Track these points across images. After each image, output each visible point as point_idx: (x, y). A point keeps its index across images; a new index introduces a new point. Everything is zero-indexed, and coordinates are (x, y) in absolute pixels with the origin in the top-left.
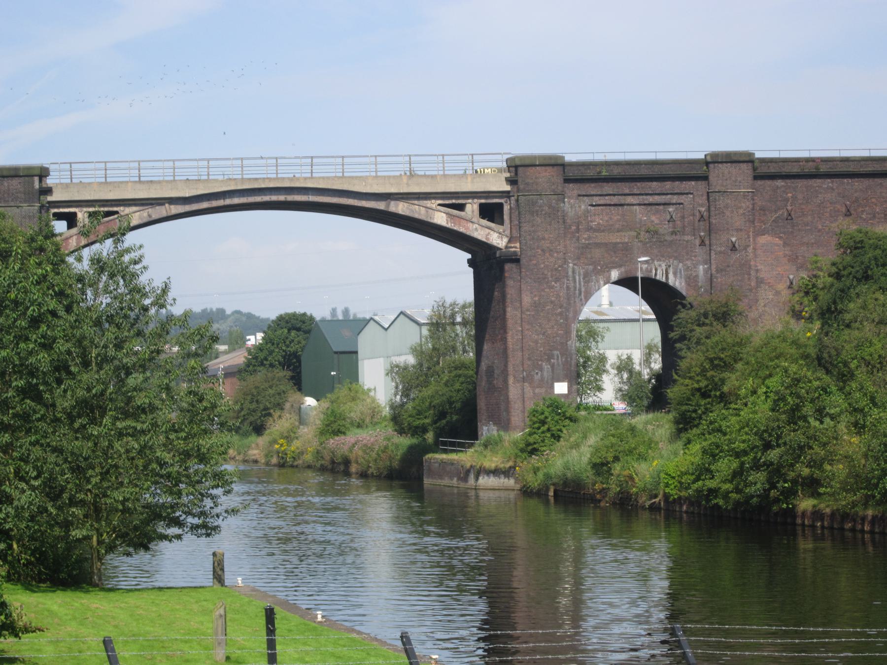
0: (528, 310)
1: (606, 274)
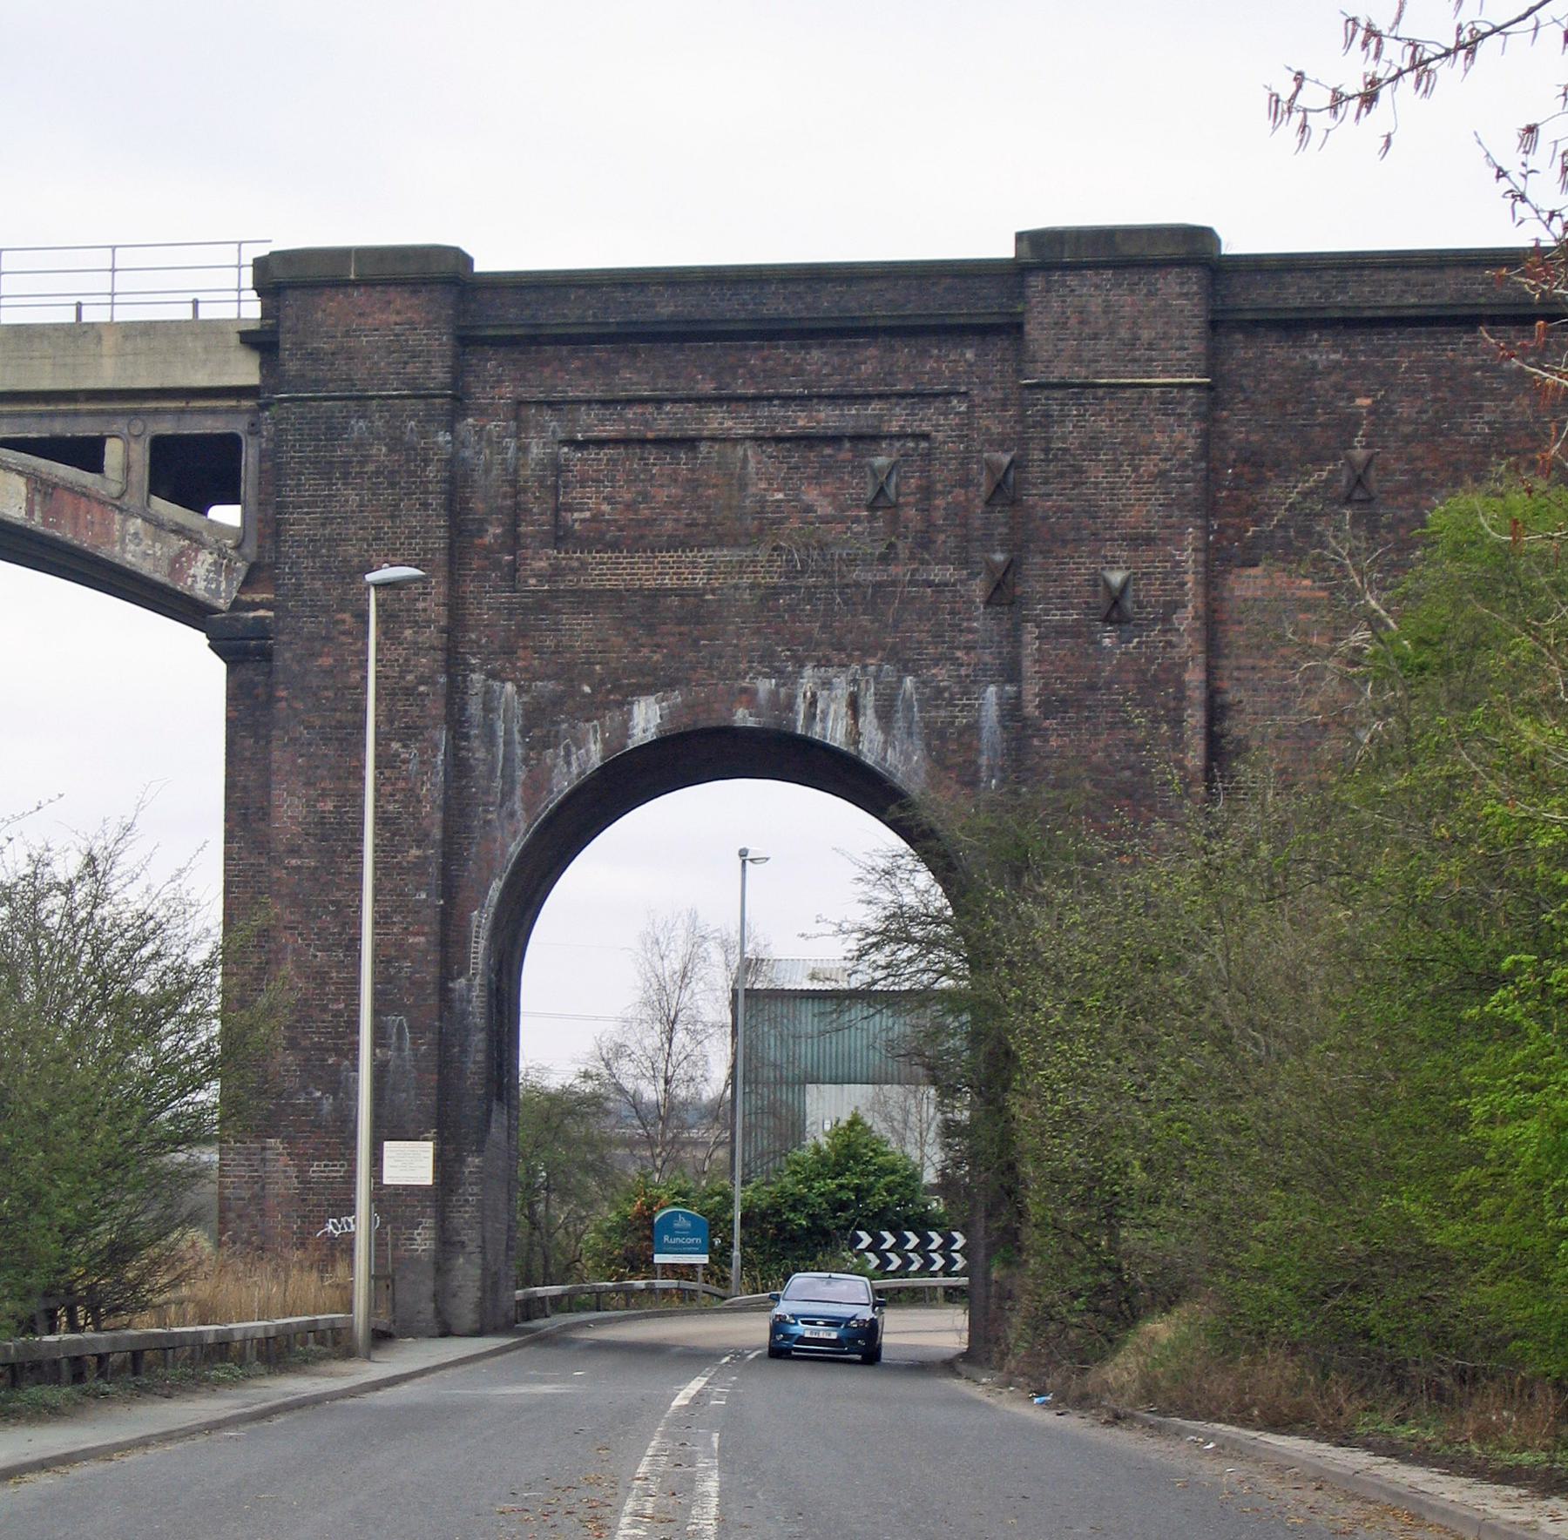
0: (294, 851)
1: (613, 717)
